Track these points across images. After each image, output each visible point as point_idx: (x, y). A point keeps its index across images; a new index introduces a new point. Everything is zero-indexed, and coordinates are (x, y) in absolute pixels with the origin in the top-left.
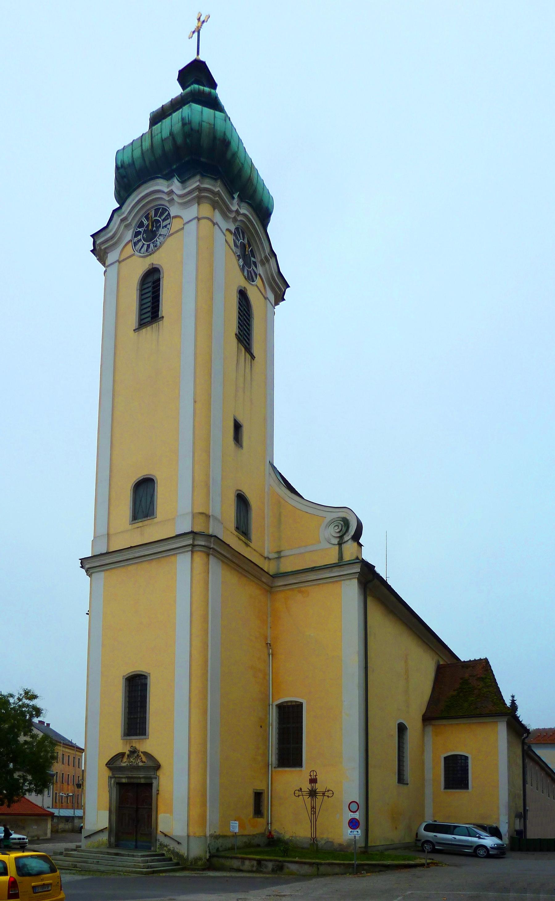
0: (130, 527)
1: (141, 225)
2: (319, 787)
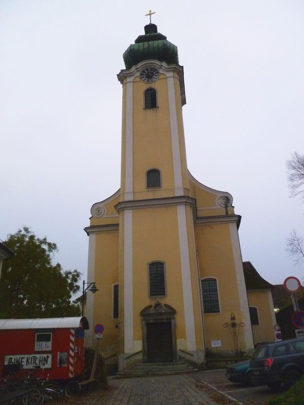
0: (146, 190)
1: (144, 72)
2: (237, 321)
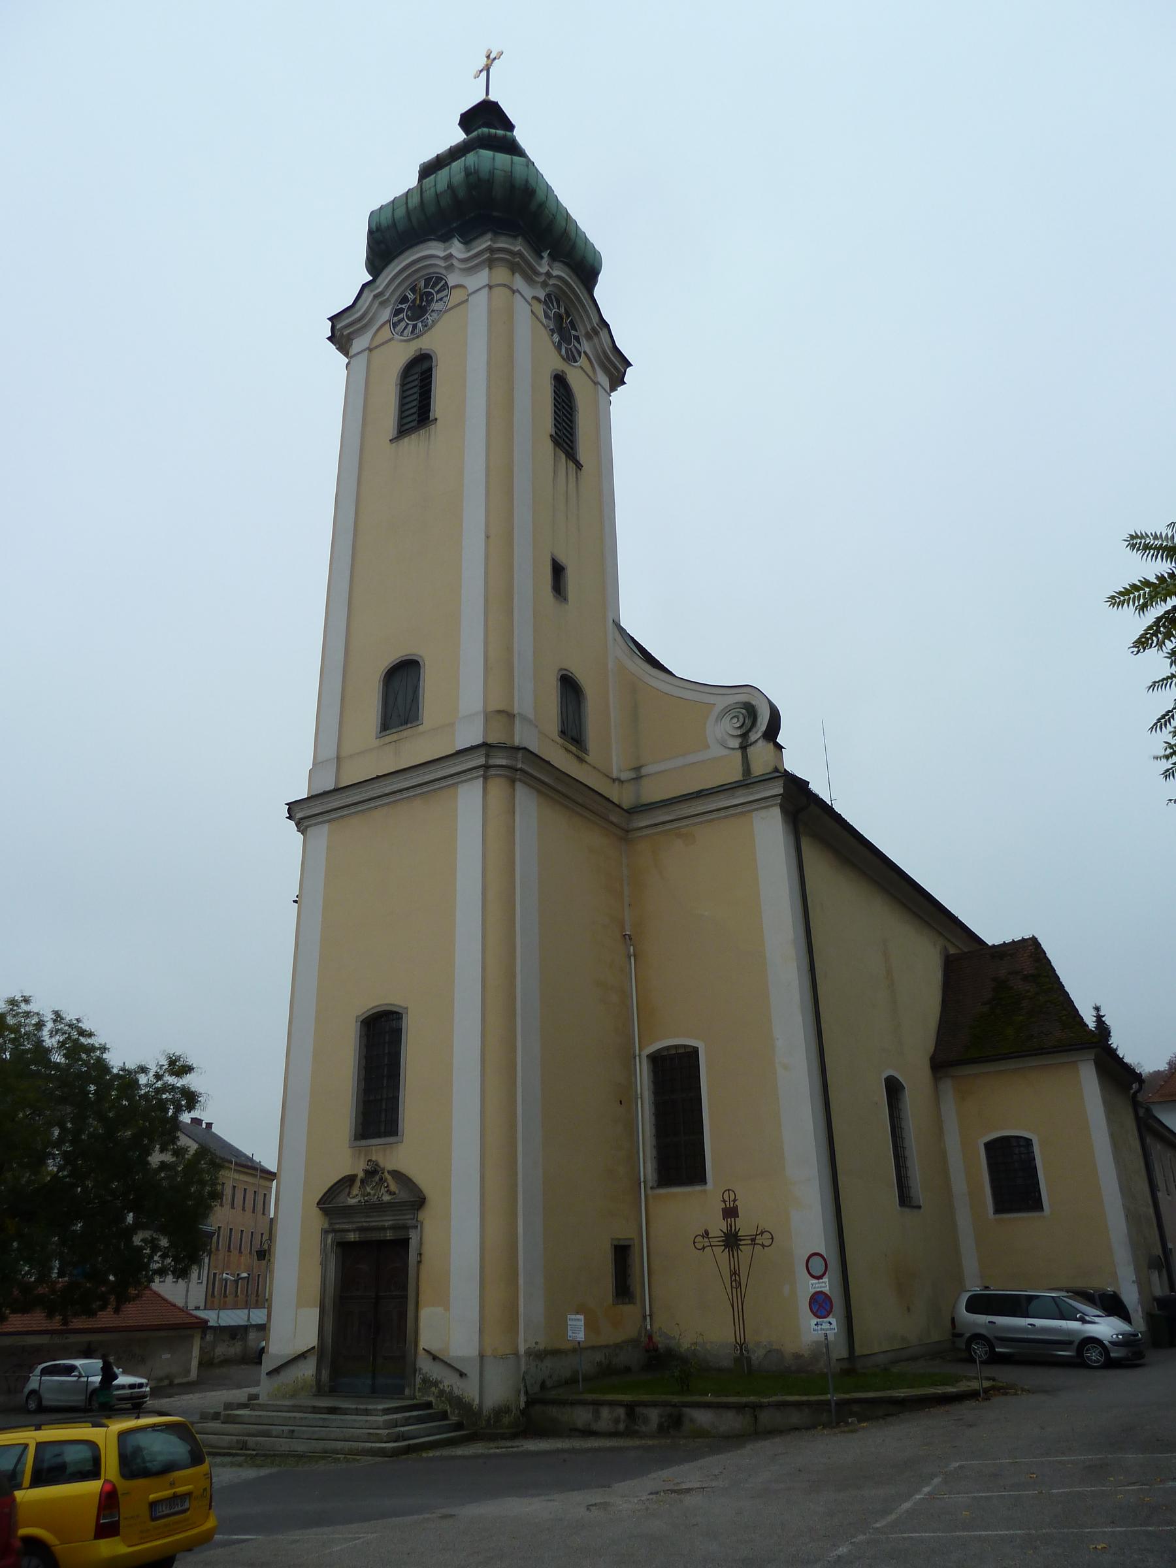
0: (376, 743)
1: (404, 299)
2: (744, 1225)
